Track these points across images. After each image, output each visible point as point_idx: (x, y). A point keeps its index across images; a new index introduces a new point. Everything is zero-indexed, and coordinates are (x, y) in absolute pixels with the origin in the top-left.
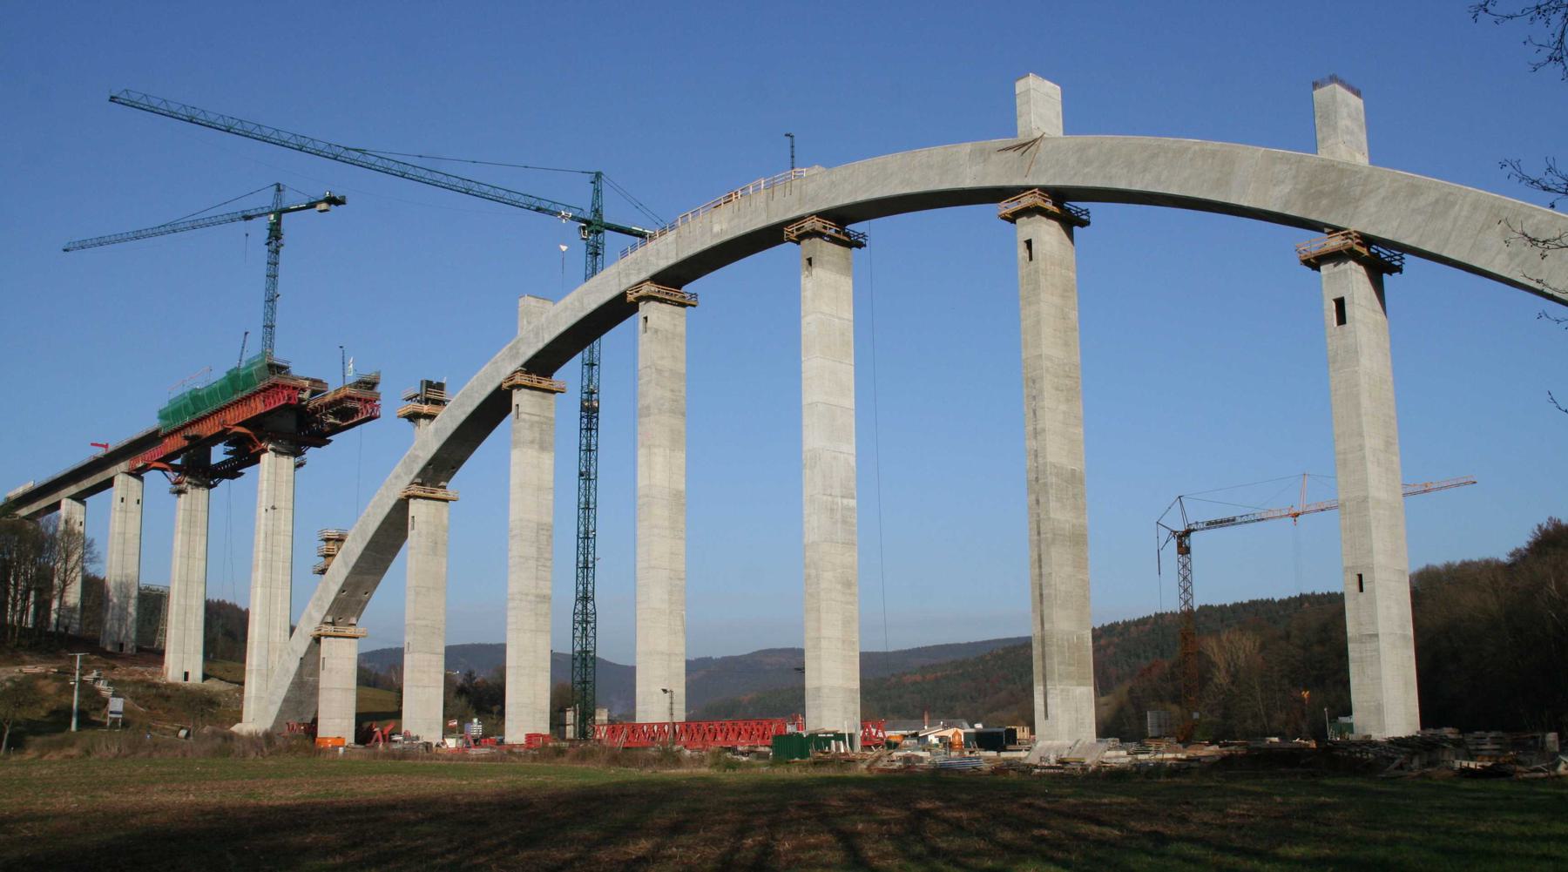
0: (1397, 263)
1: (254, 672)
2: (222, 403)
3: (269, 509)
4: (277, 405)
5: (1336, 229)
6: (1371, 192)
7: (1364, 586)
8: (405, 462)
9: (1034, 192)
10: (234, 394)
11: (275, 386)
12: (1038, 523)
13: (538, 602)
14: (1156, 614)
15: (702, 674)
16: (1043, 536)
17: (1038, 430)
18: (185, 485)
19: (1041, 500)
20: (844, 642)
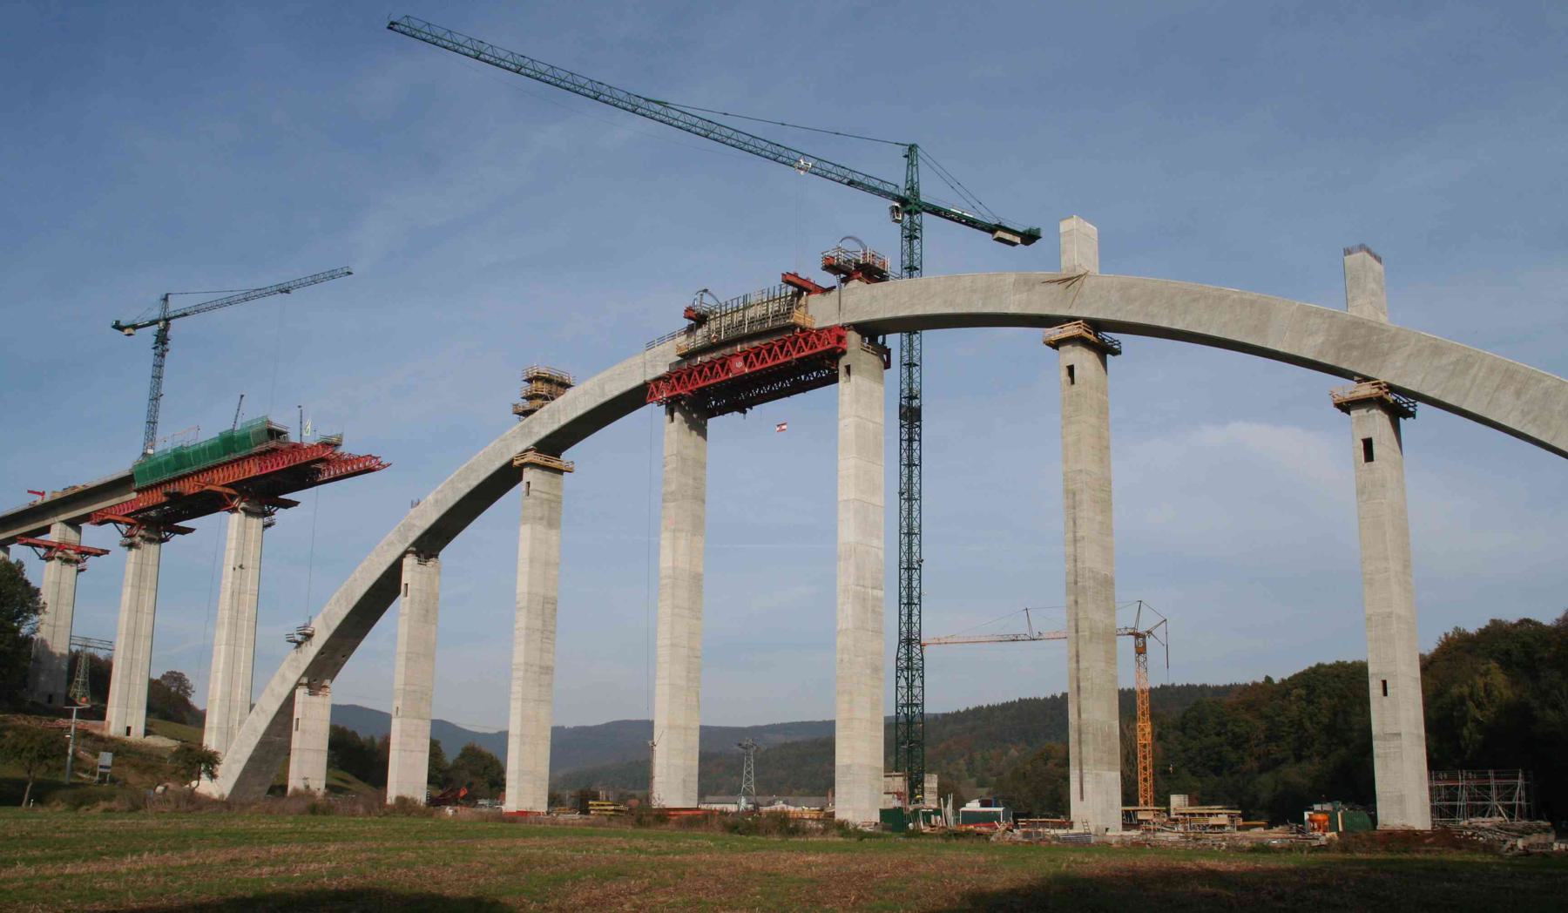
0: (1411, 409)
1: (215, 729)
2: (211, 463)
3: (237, 568)
4: (275, 469)
5: (1366, 379)
6: (1399, 348)
7: (1389, 691)
8: (399, 531)
9: (1079, 324)
10: (225, 455)
11: (274, 450)
12: (1077, 621)
13: (541, 673)
14: (1020, 699)
15: (565, 743)
16: (1080, 634)
17: (1078, 538)
18: (137, 539)
19: (1080, 601)
20: (871, 723)
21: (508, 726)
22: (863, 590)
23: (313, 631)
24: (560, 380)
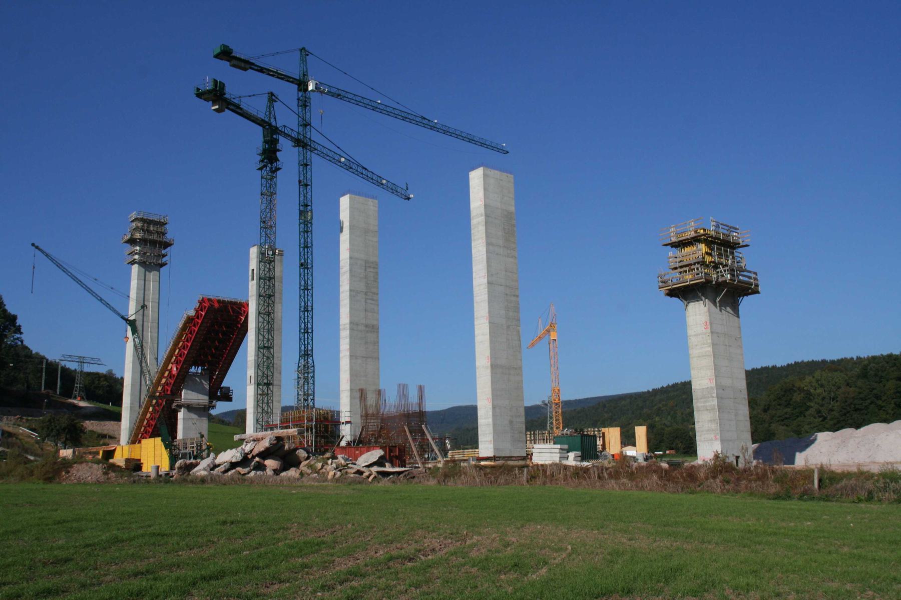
24: (708, 313)
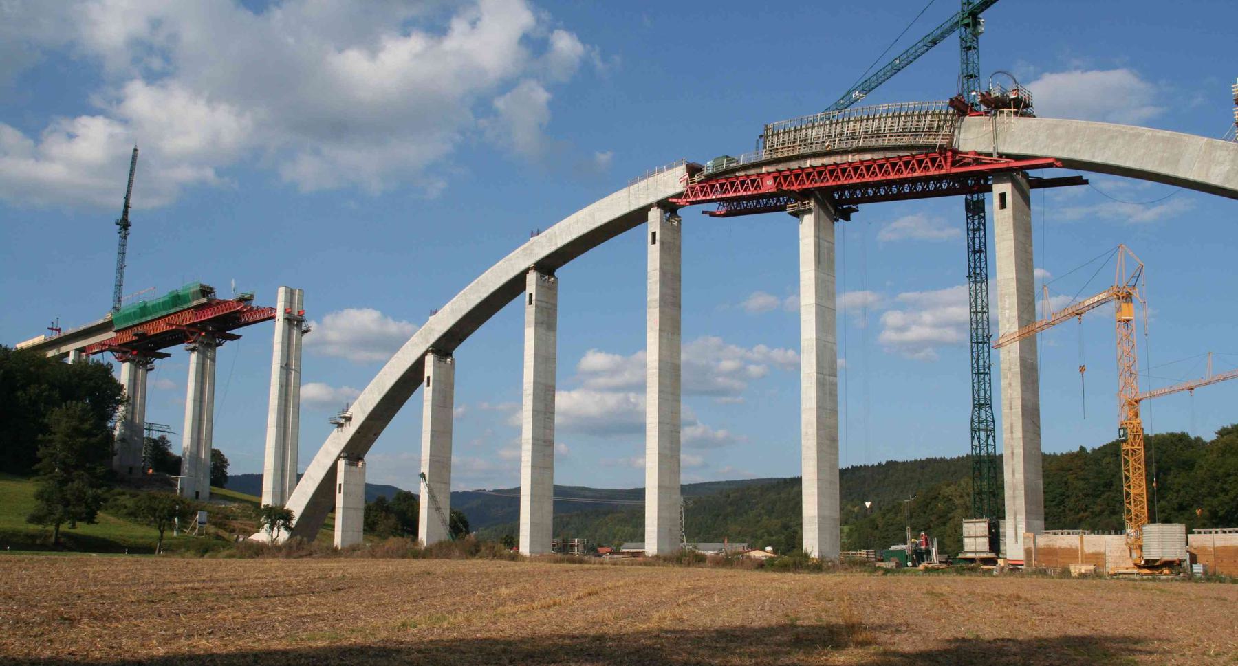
21: (644, 482)
22: (822, 376)
23: (351, 415)
